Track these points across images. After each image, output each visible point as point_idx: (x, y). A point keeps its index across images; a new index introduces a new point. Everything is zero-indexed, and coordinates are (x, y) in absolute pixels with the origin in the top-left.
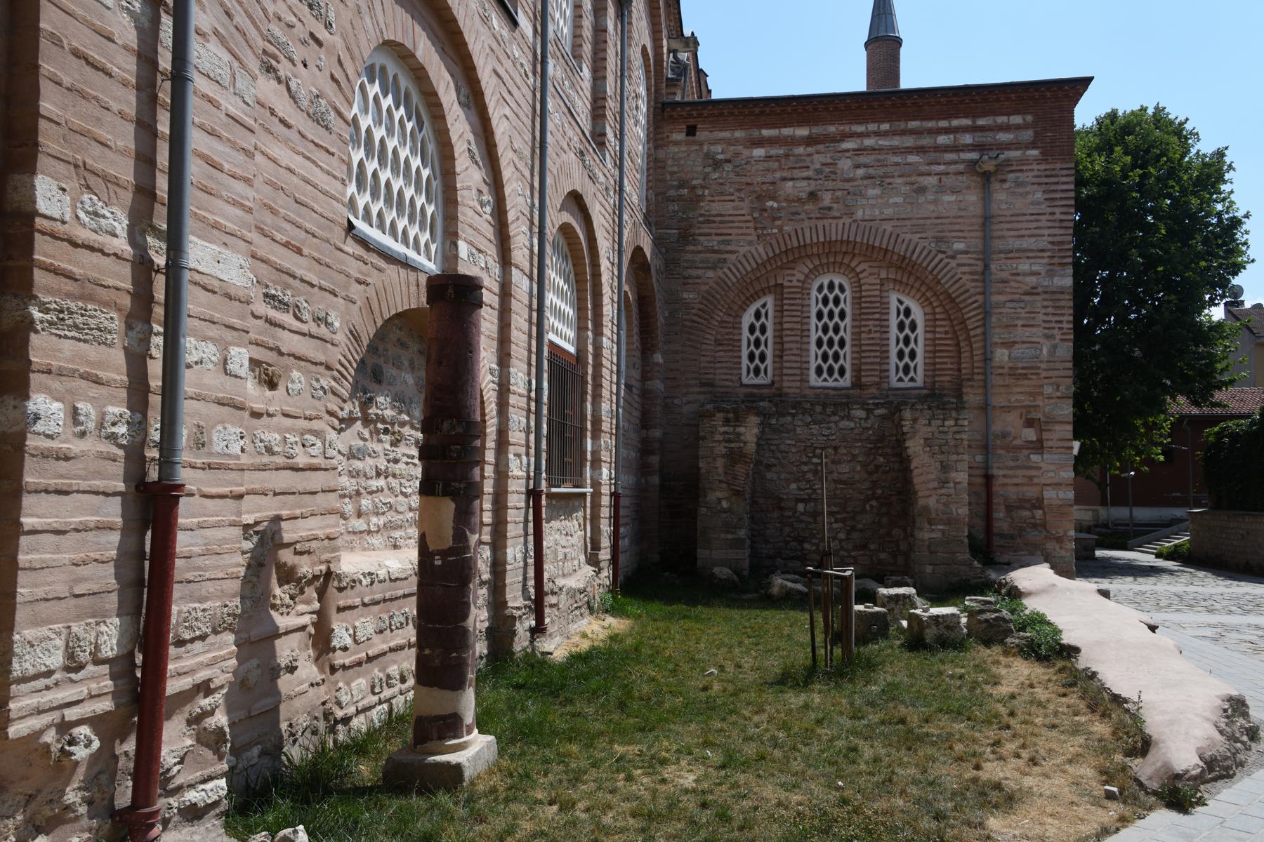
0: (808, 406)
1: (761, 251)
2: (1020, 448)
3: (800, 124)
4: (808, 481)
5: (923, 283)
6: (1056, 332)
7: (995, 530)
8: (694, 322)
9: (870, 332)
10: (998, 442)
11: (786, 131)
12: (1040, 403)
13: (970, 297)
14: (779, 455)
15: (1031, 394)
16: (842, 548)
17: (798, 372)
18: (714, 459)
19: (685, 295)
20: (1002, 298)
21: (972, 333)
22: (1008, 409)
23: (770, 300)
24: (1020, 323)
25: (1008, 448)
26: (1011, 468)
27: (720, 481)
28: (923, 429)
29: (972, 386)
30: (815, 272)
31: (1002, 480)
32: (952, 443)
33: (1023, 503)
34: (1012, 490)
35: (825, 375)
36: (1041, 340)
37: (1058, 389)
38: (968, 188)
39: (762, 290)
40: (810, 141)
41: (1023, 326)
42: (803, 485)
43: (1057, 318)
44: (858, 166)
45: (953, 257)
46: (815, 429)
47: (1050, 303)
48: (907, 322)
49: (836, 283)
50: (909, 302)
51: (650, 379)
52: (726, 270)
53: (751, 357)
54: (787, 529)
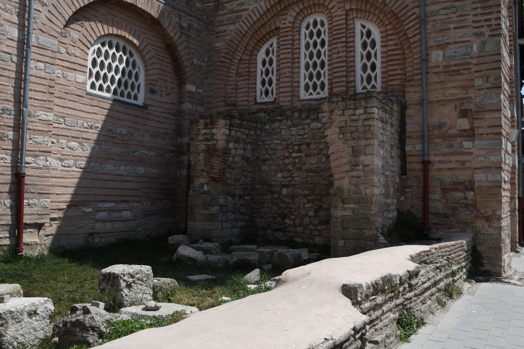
0: (289, 113)
2: (455, 136)
4: (289, 171)
5: (376, 8)
6: (485, 29)
7: (432, 210)
8: (222, 62)
9: (338, 52)
10: (436, 132)
12: (471, 95)
13: (409, 11)
14: (270, 152)
15: (464, 88)
16: (311, 223)
17: (289, 89)
18: (199, 154)
19: (217, 45)
20: (436, 7)
21: (411, 40)
22: (443, 102)
24: (452, 26)
25: (444, 137)
26: (446, 155)
27: (202, 171)
28: (338, 119)
29: (413, 86)
30: (302, 15)
31: (437, 166)
32: (361, 129)
33: (457, 186)
34: (448, 173)
35: (311, 90)
36: (471, 39)
37: (487, 81)
39: (268, 33)
41: (454, 28)
42: (285, 174)
43: (486, 17)
48: (369, 41)
49: (318, 20)
50: (370, 26)
51: (183, 103)
52: (241, 23)
53: (263, 83)
54: (275, 208)
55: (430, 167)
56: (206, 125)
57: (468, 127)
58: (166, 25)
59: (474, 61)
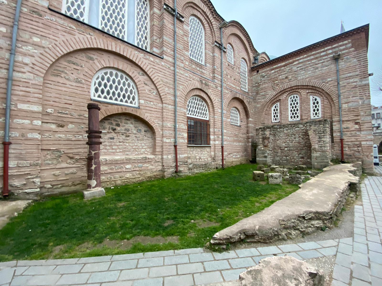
1: (275, 93)
3: (282, 62)
7: (344, 154)
11: (279, 65)
23: (278, 103)
38: (331, 64)
40: (284, 66)
44: (297, 68)
45: (327, 83)
46: (289, 131)
47: (361, 89)
55: (344, 141)
56: (262, 130)
57: (358, 128)
58: (245, 102)
59: (360, 107)
